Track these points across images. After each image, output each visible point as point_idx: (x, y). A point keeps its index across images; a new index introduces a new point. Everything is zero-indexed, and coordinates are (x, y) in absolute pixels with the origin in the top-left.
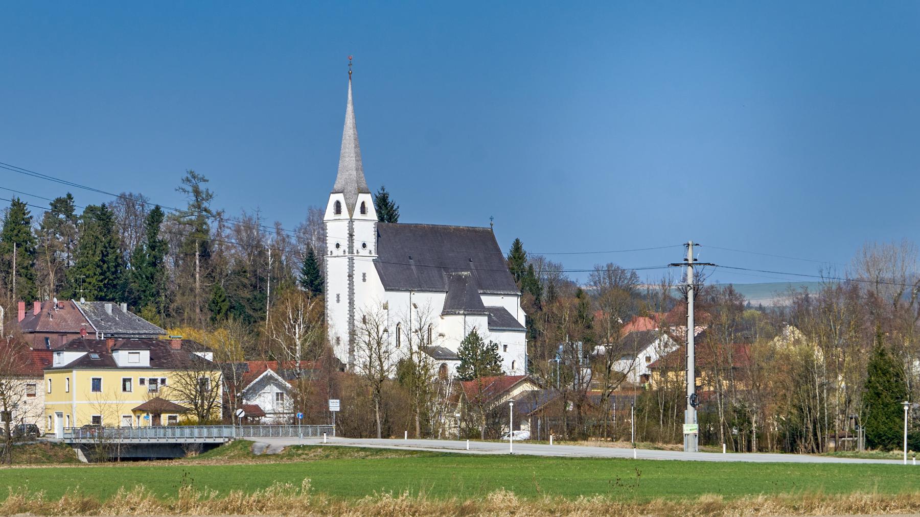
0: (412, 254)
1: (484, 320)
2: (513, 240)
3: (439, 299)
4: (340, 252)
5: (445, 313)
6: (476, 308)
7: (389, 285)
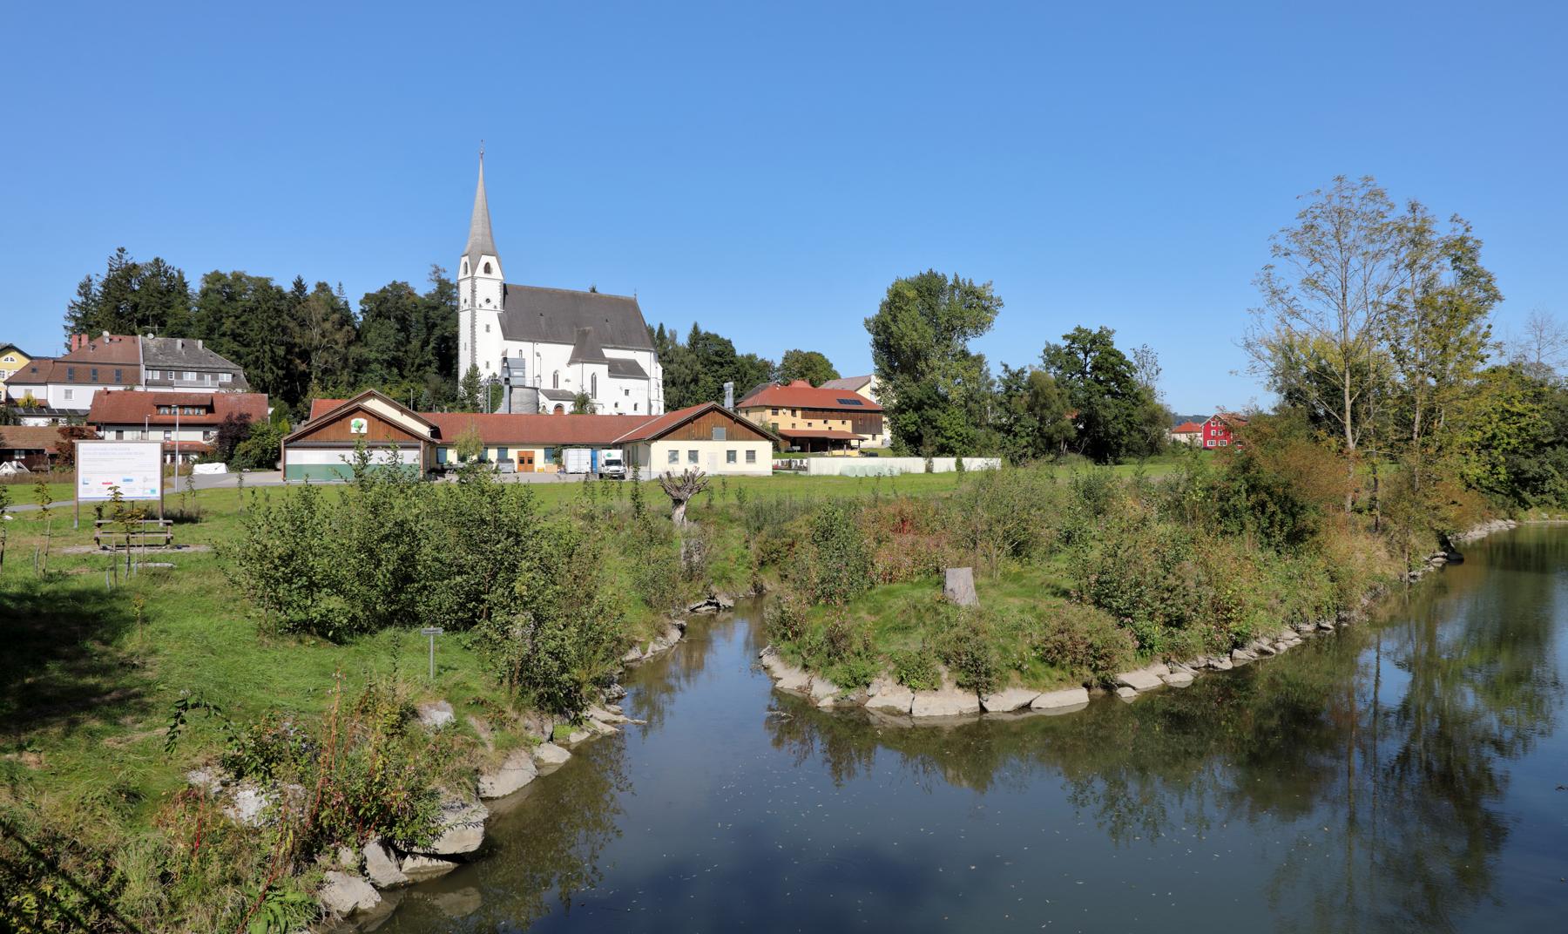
0: (527, 314)
1: (606, 367)
2: (295, 279)
3: (567, 350)
4: (490, 306)
5: (572, 361)
6: (600, 359)
7: (509, 333)
